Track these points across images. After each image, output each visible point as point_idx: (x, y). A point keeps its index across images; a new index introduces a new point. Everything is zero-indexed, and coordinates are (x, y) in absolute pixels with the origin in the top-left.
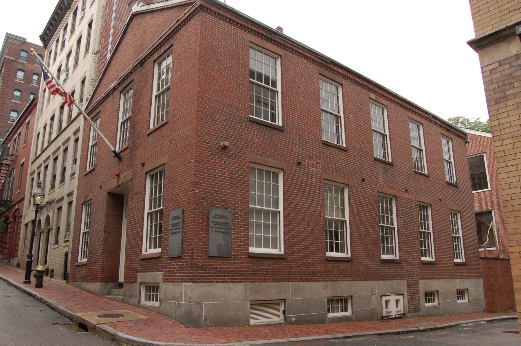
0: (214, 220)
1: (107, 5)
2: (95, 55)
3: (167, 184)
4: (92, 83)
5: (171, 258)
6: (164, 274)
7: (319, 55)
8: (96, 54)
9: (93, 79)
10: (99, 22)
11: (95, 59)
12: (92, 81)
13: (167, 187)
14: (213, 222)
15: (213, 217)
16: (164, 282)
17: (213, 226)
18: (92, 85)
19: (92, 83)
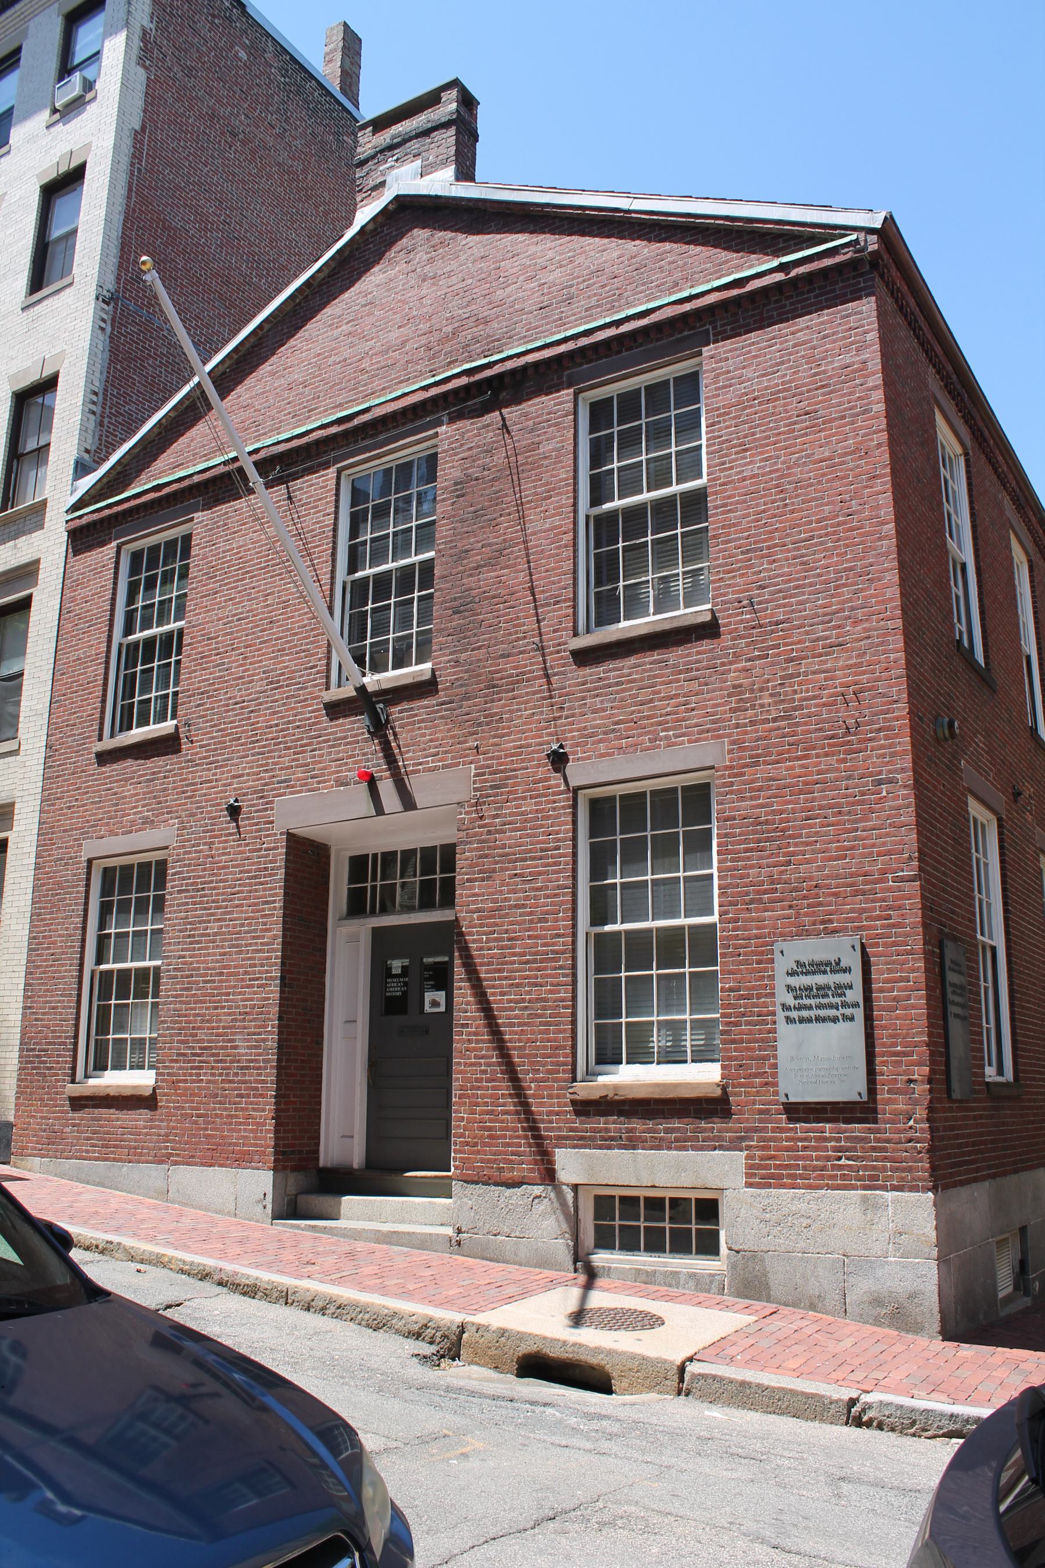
0: (795, 981)
1: (143, 128)
2: (105, 306)
3: (58, 718)
4: (94, 408)
5: (797, 1112)
6: (747, 1157)
7: (998, 435)
8: (108, 304)
9: (96, 394)
10: (119, 187)
11: (103, 320)
12: (95, 398)
13: (55, 723)
14: (789, 988)
15: (851, 987)
16: (749, 1185)
17: (791, 1001)
18: (93, 413)
19: (94, 408)
